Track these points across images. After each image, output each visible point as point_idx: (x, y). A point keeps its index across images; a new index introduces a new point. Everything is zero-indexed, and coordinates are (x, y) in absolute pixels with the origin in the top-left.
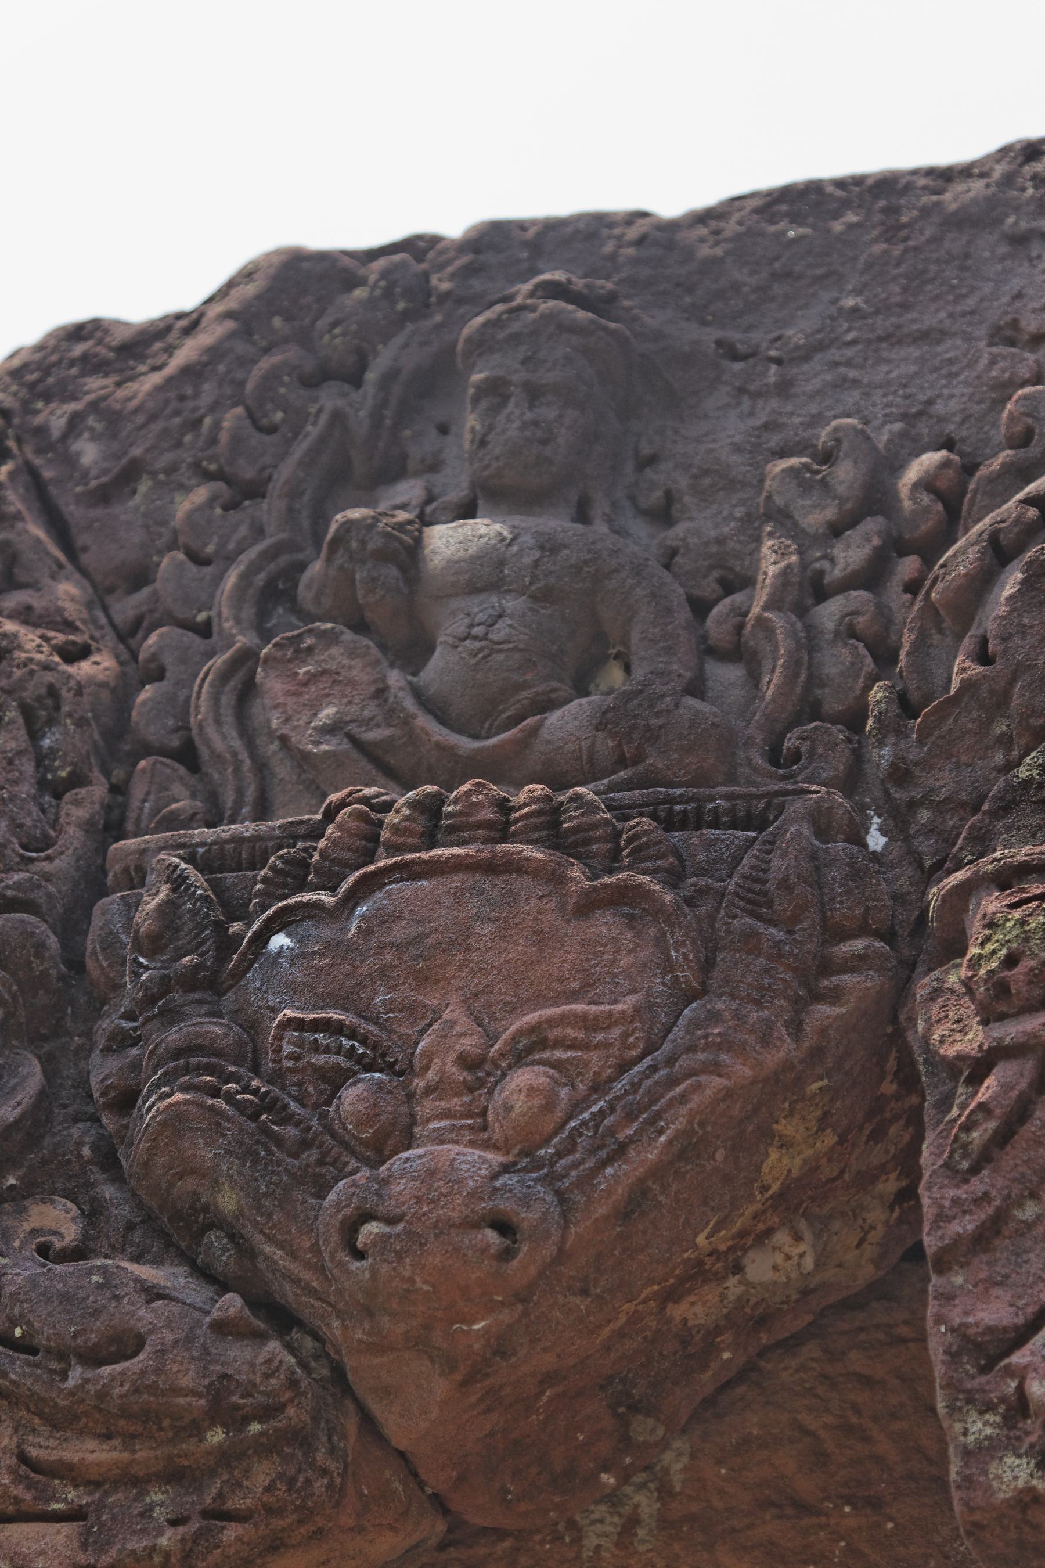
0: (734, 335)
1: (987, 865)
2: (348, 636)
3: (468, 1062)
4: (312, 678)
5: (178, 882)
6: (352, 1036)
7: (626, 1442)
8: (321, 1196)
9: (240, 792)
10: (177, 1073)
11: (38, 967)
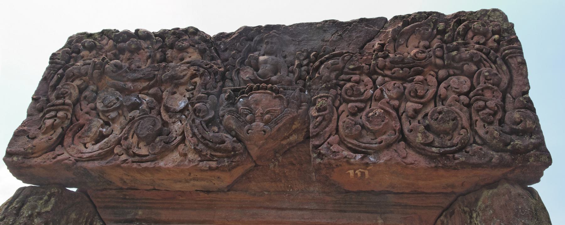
0: (294, 39)
1: (319, 96)
2: (250, 68)
3: (261, 114)
4: (246, 72)
5: (230, 93)
6: (249, 110)
7: (275, 156)
8: (244, 127)
9: (237, 84)
10: (229, 113)
11: (215, 101)
